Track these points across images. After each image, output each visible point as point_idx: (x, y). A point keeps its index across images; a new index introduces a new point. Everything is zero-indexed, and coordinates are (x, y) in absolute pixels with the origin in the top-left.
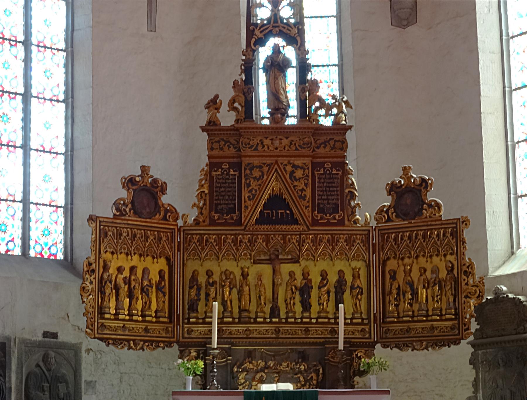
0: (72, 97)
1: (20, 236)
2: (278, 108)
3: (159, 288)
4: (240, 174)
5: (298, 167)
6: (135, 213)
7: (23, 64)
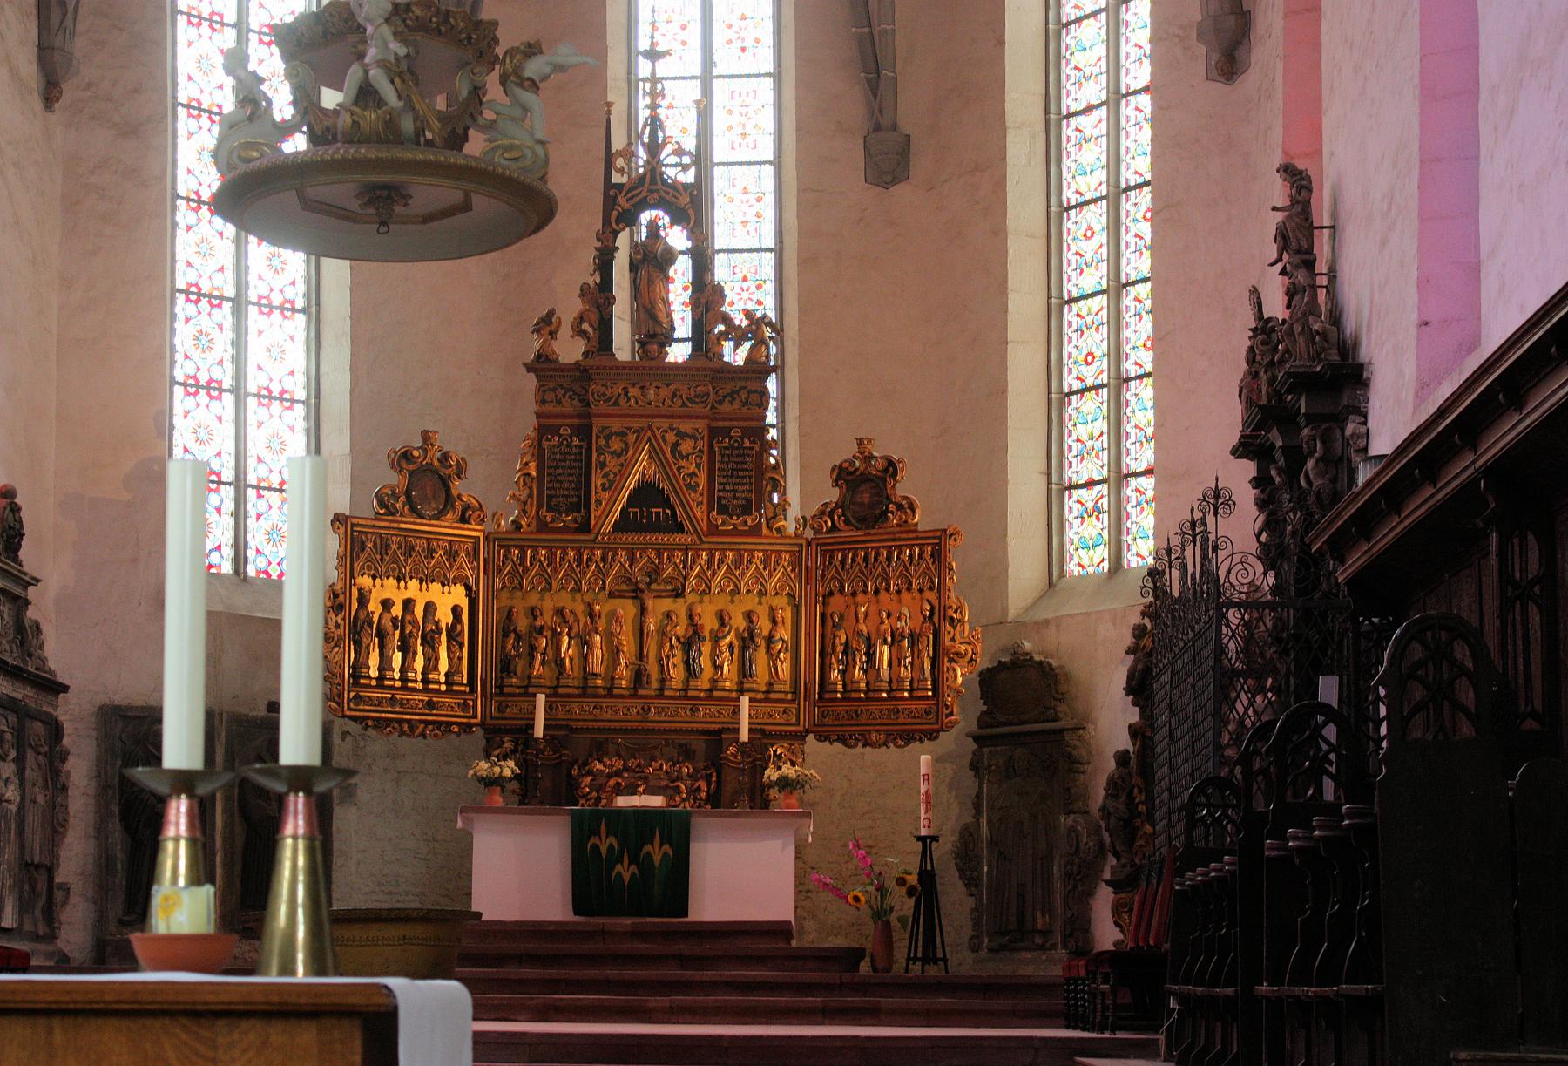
0: (318, 304)
1: (231, 541)
2: (654, 334)
3: (453, 634)
4: (590, 444)
5: (686, 435)
6: (413, 510)
7: (233, 246)
